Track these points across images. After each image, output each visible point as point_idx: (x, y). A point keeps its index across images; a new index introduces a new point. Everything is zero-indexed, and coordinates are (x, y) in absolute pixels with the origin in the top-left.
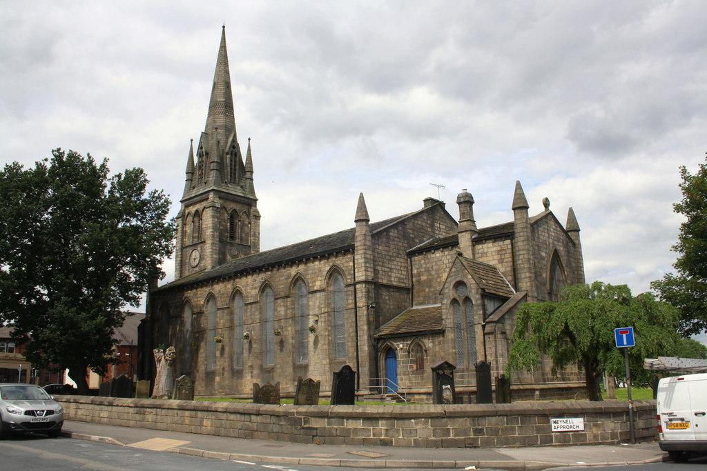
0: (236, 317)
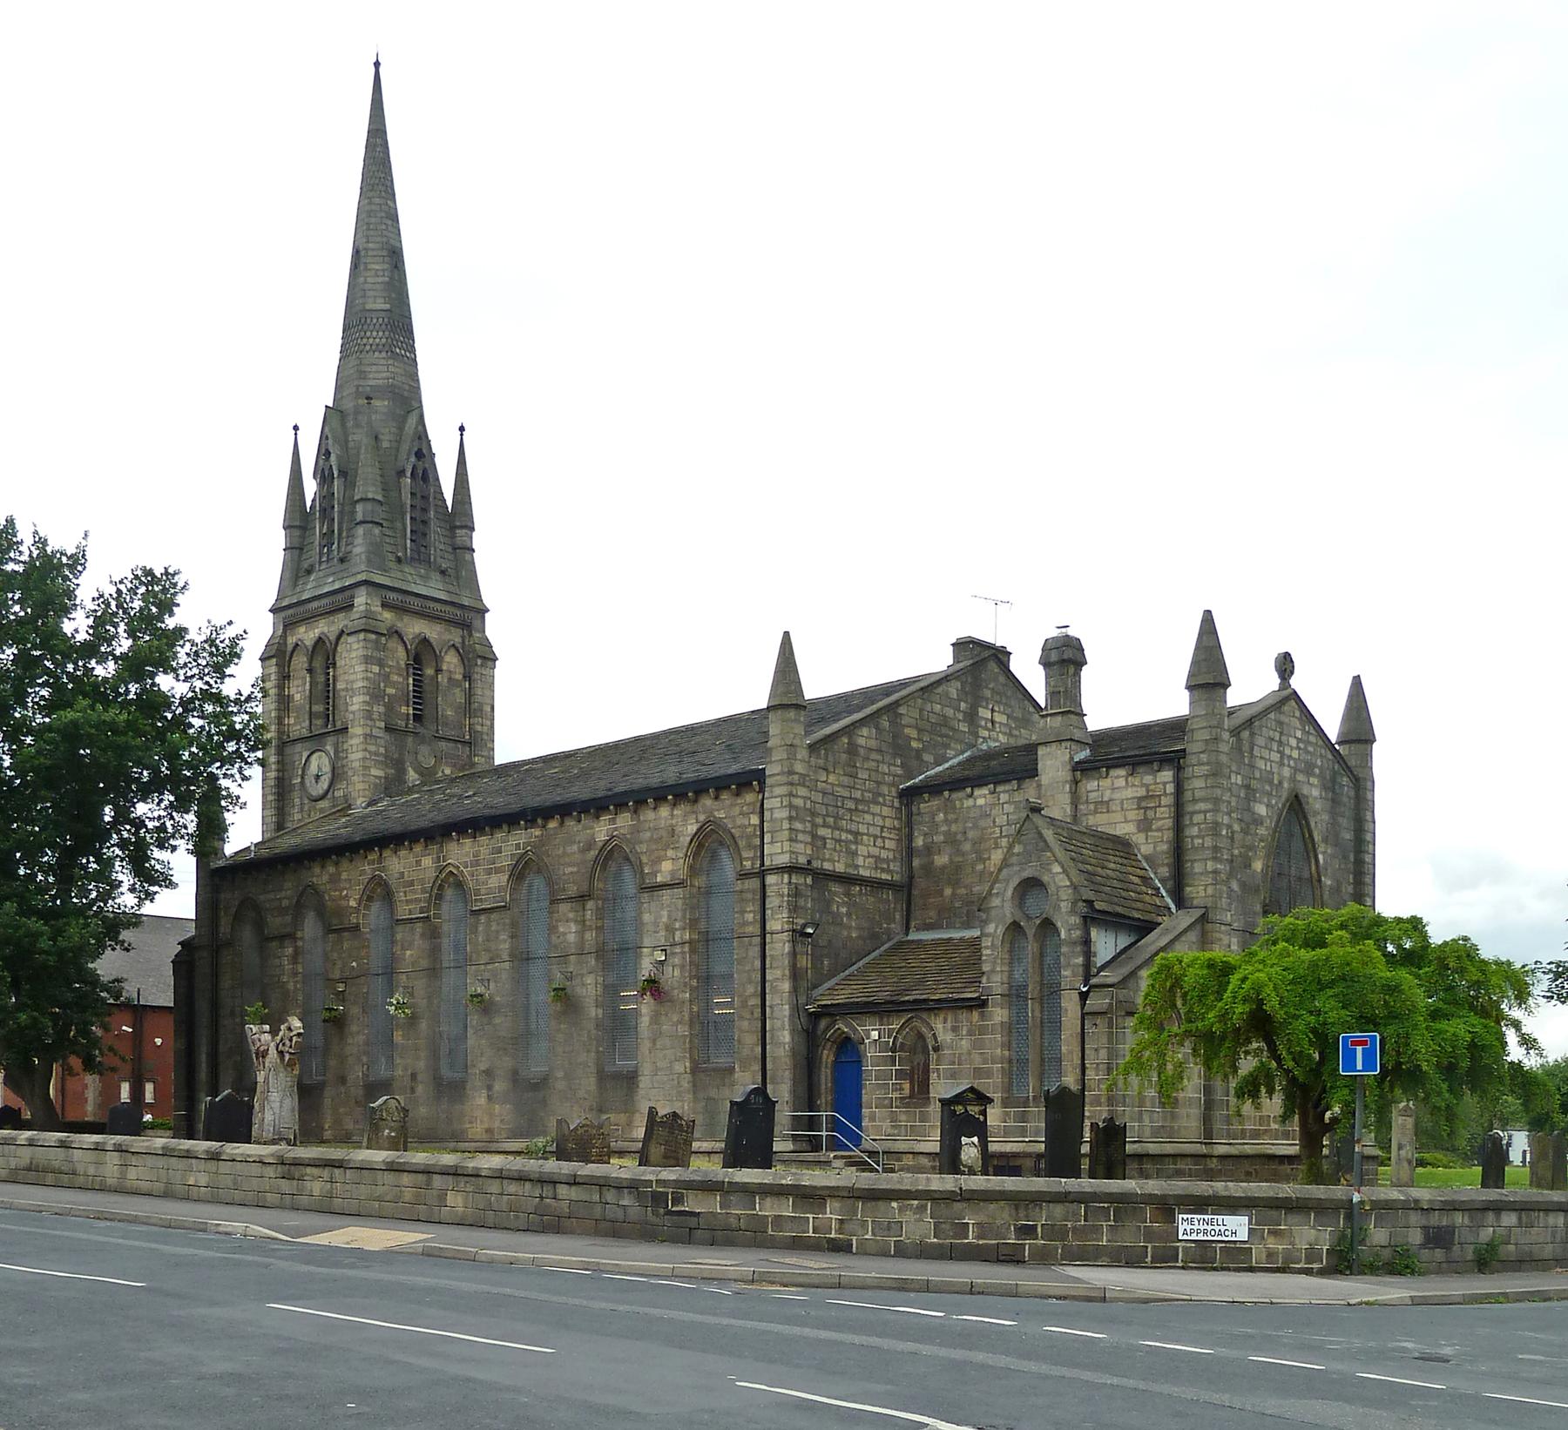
0: (446, 943)
